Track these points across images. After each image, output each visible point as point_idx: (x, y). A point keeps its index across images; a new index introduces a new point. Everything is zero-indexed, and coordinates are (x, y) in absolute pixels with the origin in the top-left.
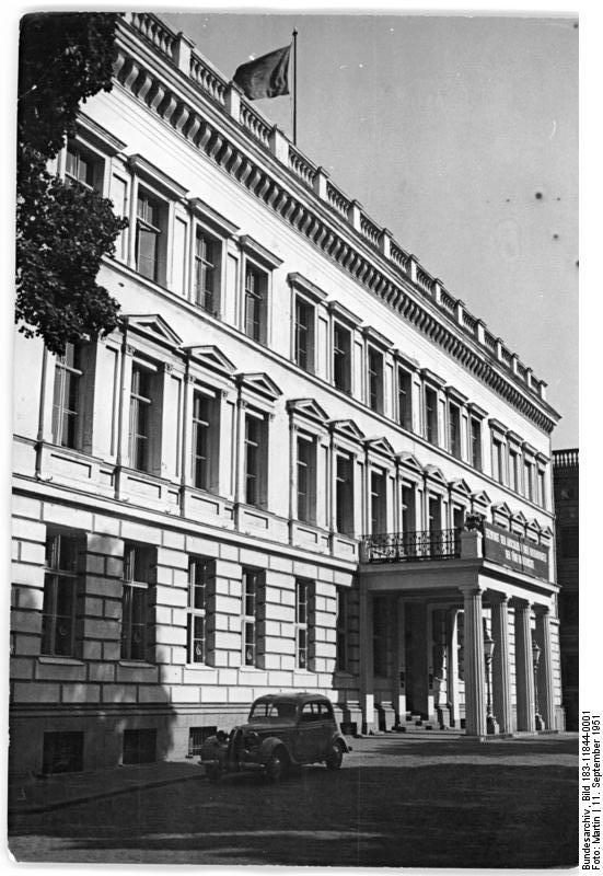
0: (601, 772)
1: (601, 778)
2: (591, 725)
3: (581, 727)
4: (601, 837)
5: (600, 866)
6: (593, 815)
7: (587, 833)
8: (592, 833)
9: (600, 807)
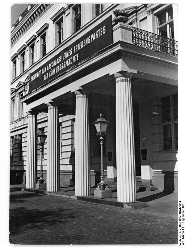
0: (184, 219)
1: (184, 220)
2: (182, 205)
3: (179, 206)
4: (184, 237)
5: (184, 245)
6: (182, 231)
7: (181, 236)
8: (182, 236)
9: (184, 228)
